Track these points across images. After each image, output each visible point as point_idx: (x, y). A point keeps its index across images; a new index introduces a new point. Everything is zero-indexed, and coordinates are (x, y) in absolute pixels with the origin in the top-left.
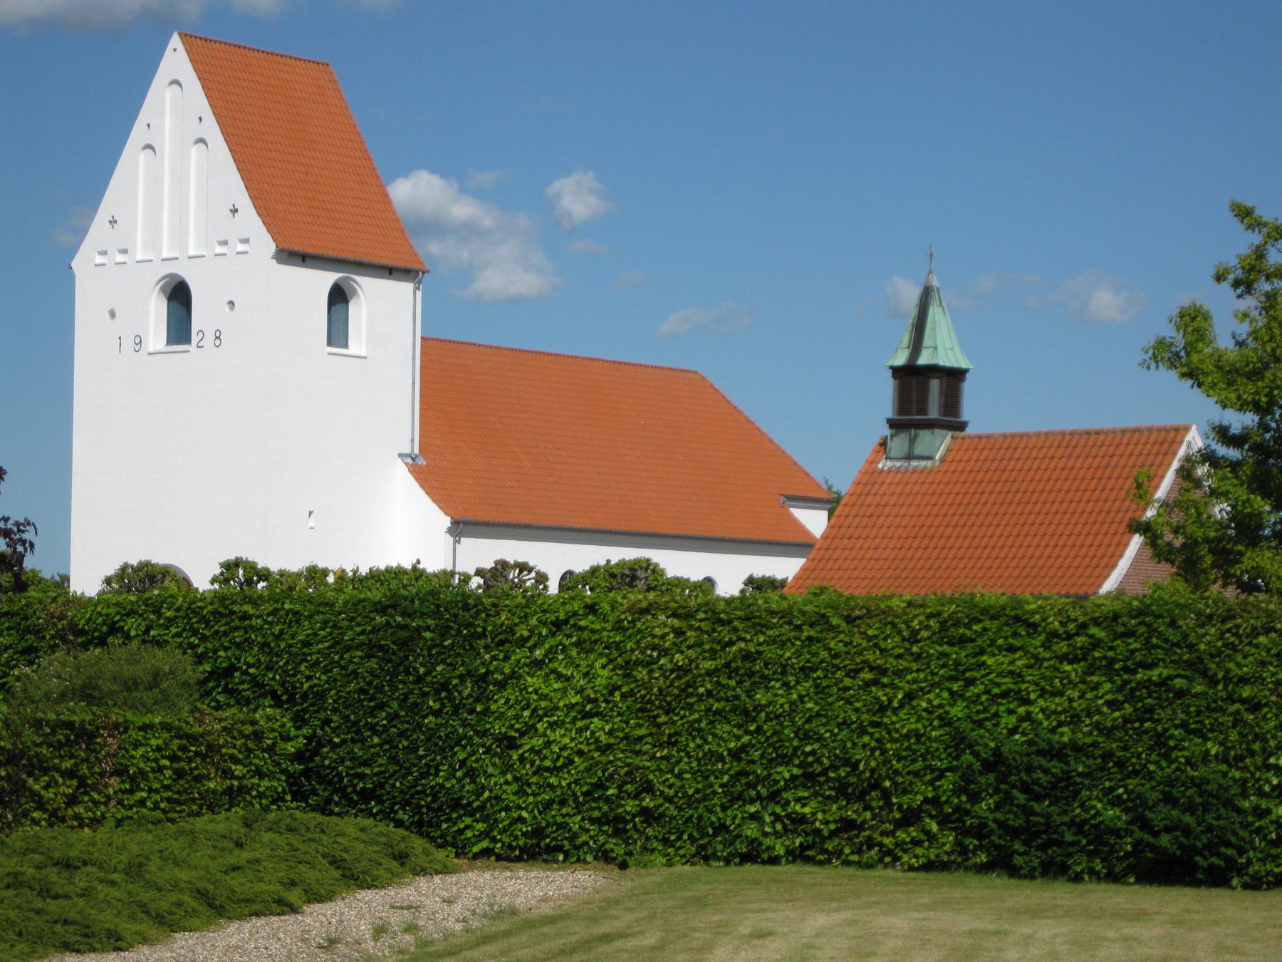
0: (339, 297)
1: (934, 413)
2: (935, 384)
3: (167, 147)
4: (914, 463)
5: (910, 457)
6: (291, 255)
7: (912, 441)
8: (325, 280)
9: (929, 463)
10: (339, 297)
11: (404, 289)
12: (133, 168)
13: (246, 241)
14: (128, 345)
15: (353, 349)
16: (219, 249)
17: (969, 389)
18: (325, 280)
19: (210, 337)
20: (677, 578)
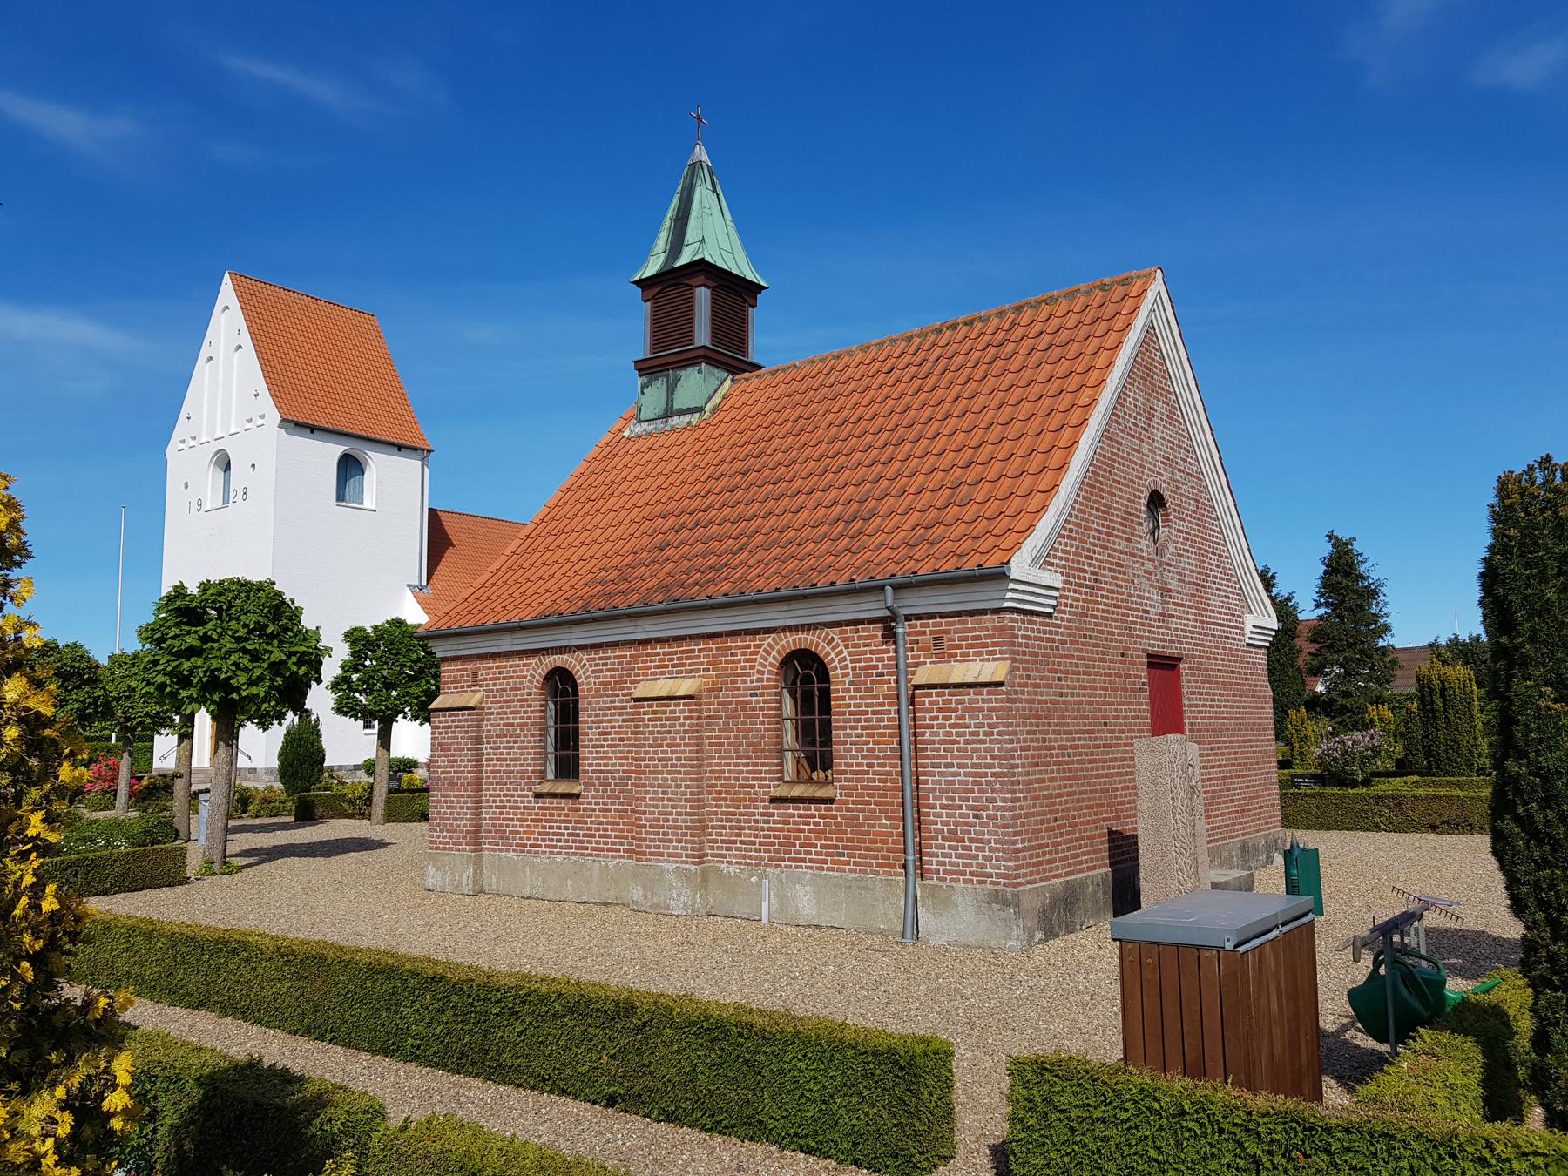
0: (350, 467)
1: (702, 336)
2: (703, 296)
3: (220, 359)
4: (674, 421)
5: (669, 413)
6: (296, 425)
7: (671, 390)
8: (336, 450)
9: (695, 418)
10: (350, 467)
11: (410, 467)
12: (203, 375)
13: (262, 417)
14: (195, 506)
15: (367, 504)
16: (248, 426)
17: (759, 318)
18: (336, 450)
19: (240, 493)
20: (237, 582)
